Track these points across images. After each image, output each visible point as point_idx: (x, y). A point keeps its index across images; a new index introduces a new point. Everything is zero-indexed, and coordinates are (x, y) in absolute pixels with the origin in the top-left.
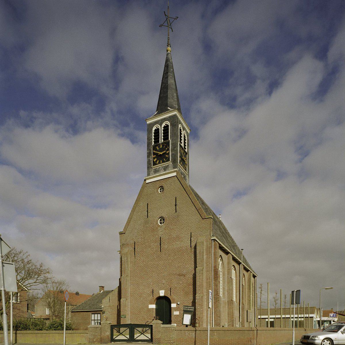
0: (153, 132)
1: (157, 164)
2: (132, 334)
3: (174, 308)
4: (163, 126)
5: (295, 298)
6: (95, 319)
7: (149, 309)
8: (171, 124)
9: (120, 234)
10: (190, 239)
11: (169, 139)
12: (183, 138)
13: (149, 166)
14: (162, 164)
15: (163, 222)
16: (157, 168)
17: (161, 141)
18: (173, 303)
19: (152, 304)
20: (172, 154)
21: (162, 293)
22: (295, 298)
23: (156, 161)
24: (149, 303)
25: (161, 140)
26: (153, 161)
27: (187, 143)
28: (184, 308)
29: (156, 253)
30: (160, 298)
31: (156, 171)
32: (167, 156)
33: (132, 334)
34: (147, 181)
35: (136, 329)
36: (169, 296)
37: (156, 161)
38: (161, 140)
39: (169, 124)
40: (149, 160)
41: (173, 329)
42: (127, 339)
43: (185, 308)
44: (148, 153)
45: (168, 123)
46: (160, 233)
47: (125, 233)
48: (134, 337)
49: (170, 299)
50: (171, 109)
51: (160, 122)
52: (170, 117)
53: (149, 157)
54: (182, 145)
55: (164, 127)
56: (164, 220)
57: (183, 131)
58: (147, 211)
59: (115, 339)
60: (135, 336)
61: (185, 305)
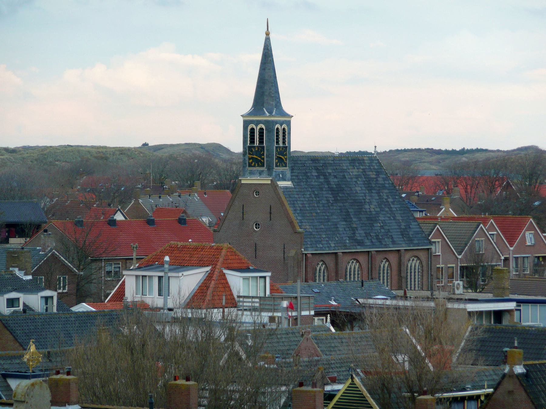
0: (249, 130)
3: (167, 264)
5: (535, 225)
8: (266, 129)
14: (257, 168)
15: (258, 195)
20: (267, 161)
22: (535, 225)
23: (252, 163)
26: (249, 163)
28: (415, 290)
31: (251, 173)
37: (252, 163)
38: (257, 143)
39: (264, 128)
40: (245, 159)
43: (415, 287)
45: (264, 127)
46: (255, 239)
47: (219, 232)
52: (265, 121)
56: (258, 192)
58: (243, 213)
61: (367, 278)
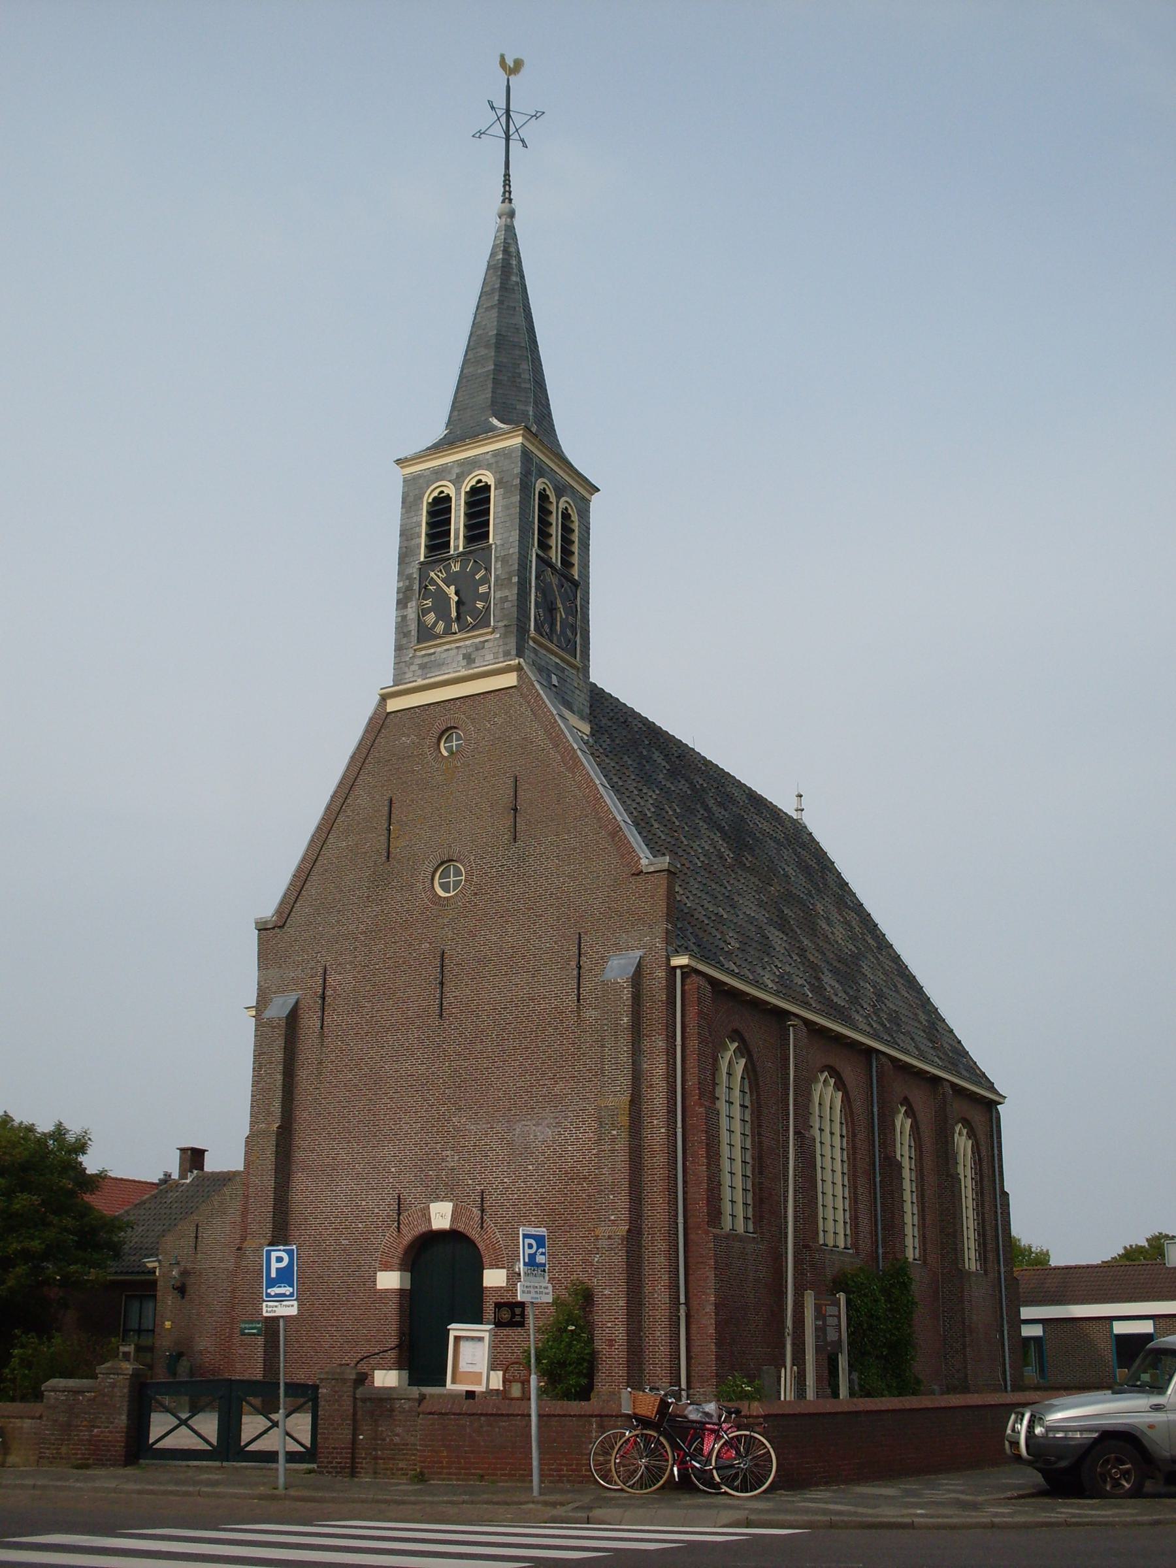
1: (438, 637)
2: (230, 1429)
4: (467, 486)
6: (144, 1327)
7: (376, 1291)
9: (259, 930)
10: (573, 964)
11: (491, 541)
12: (555, 531)
13: (404, 641)
16: (439, 649)
17: (457, 547)
18: (492, 1267)
19: (386, 1267)
21: (441, 1216)
24: (377, 1265)
25: (457, 541)
27: (576, 540)
29: (418, 1022)
30: (431, 1239)
32: (480, 605)
33: (230, 1429)
34: (393, 705)
35: (248, 1403)
36: (474, 1234)
38: (457, 541)
41: (406, 1407)
42: (302, 1449)
44: (399, 590)
45: (489, 478)
48: (148, 1438)
49: (481, 1246)
50: (502, 426)
51: (456, 470)
52: (496, 453)
53: (407, 607)
54: (555, 556)
55: (474, 491)
57: (558, 497)
59: (247, 1449)
60: (155, 1433)
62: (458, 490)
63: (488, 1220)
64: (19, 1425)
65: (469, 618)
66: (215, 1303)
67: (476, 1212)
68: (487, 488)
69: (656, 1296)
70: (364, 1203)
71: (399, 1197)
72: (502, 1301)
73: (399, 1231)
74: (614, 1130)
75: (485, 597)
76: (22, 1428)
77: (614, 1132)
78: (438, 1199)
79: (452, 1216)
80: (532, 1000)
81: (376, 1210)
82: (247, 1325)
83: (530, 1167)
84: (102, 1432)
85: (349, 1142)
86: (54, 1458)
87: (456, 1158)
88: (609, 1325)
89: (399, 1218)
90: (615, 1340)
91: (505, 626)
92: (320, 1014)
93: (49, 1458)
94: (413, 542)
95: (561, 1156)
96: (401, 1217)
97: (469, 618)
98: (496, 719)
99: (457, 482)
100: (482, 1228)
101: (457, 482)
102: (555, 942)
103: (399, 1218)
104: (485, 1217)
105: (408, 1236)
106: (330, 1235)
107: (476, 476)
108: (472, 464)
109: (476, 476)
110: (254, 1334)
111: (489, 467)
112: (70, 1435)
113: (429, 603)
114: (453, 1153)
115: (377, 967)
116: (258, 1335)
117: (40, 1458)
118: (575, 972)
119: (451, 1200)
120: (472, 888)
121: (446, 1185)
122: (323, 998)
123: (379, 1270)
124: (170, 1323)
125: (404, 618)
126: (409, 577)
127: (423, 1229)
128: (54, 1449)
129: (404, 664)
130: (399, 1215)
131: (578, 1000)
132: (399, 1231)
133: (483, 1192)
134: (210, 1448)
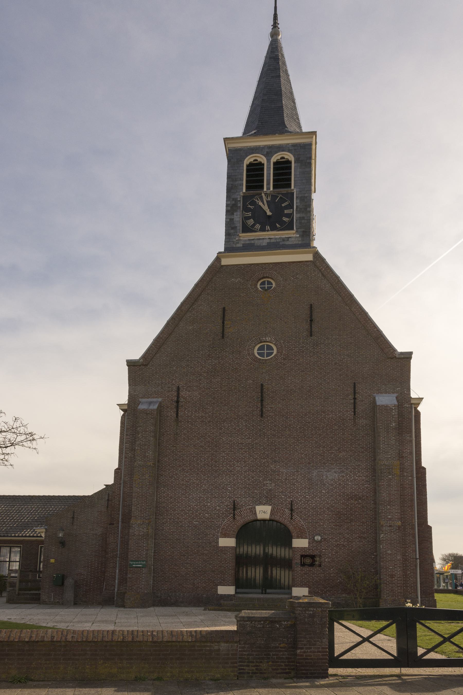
7: (218, 547)
11: (293, 187)
17: (269, 188)
18: (298, 537)
19: (225, 535)
34: (225, 262)
45: (290, 157)
51: (267, 150)
62: (269, 161)
63: (296, 515)
64: (216, 648)
65: (277, 225)
66: (87, 550)
67: (288, 512)
68: (289, 162)
69: (407, 555)
70: (209, 504)
71: (234, 501)
72: (306, 554)
73: (234, 519)
74: (390, 475)
75: (290, 216)
76: (219, 650)
77: (390, 477)
78: (260, 504)
79: (271, 512)
80: (324, 412)
81: (218, 508)
82: (135, 563)
83: (324, 491)
84: (305, 652)
85: (198, 474)
86: (252, 673)
87: (273, 485)
88: (391, 567)
89: (234, 512)
90: (395, 575)
91: (303, 231)
92: (175, 410)
93: (249, 673)
94: (237, 182)
95: (344, 487)
96: (235, 512)
97: (277, 225)
98: (297, 276)
99: (268, 155)
100: (292, 519)
101: (268, 155)
102: (338, 386)
103: (234, 512)
104: (294, 514)
105: (240, 521)
106: (185, 519)
107: (282, 154)
108: (280, 148)
109: (282, 154)
110: (140, 567)
111: (289, 151)
112: (269, 655)
113: (250, 214)
114: (271, 482)
115: (216, 390)
116: (142, 568)
117: (240, 673)
118: (352, 401)
119: (270, 505)
120: (282, 356)
121: (267, 497)
122: (178, 402)
123: (220, 537)
124: (54, 560)
125: (232, 220)
126: (235, 200)
127: (251, 518)
128: (254, 666)
129: (232, 242)
130: (234, 510)
131: (355, 414)
132: (234, 519)
133: (292, 502)
134: (393, 658)
